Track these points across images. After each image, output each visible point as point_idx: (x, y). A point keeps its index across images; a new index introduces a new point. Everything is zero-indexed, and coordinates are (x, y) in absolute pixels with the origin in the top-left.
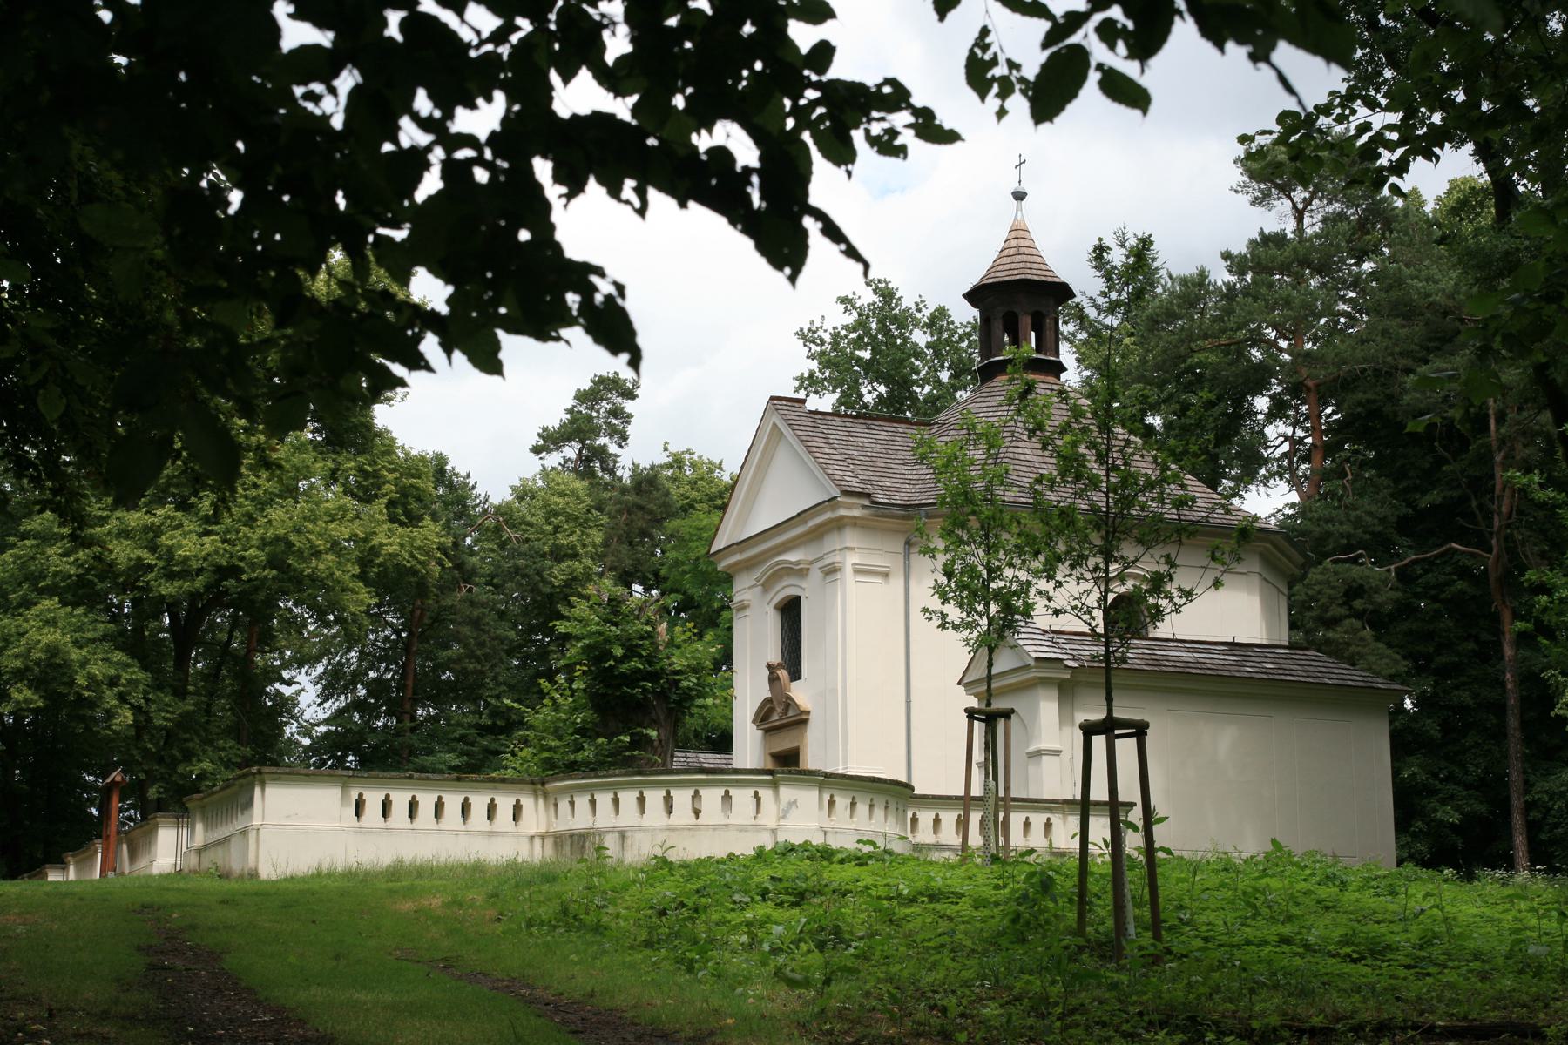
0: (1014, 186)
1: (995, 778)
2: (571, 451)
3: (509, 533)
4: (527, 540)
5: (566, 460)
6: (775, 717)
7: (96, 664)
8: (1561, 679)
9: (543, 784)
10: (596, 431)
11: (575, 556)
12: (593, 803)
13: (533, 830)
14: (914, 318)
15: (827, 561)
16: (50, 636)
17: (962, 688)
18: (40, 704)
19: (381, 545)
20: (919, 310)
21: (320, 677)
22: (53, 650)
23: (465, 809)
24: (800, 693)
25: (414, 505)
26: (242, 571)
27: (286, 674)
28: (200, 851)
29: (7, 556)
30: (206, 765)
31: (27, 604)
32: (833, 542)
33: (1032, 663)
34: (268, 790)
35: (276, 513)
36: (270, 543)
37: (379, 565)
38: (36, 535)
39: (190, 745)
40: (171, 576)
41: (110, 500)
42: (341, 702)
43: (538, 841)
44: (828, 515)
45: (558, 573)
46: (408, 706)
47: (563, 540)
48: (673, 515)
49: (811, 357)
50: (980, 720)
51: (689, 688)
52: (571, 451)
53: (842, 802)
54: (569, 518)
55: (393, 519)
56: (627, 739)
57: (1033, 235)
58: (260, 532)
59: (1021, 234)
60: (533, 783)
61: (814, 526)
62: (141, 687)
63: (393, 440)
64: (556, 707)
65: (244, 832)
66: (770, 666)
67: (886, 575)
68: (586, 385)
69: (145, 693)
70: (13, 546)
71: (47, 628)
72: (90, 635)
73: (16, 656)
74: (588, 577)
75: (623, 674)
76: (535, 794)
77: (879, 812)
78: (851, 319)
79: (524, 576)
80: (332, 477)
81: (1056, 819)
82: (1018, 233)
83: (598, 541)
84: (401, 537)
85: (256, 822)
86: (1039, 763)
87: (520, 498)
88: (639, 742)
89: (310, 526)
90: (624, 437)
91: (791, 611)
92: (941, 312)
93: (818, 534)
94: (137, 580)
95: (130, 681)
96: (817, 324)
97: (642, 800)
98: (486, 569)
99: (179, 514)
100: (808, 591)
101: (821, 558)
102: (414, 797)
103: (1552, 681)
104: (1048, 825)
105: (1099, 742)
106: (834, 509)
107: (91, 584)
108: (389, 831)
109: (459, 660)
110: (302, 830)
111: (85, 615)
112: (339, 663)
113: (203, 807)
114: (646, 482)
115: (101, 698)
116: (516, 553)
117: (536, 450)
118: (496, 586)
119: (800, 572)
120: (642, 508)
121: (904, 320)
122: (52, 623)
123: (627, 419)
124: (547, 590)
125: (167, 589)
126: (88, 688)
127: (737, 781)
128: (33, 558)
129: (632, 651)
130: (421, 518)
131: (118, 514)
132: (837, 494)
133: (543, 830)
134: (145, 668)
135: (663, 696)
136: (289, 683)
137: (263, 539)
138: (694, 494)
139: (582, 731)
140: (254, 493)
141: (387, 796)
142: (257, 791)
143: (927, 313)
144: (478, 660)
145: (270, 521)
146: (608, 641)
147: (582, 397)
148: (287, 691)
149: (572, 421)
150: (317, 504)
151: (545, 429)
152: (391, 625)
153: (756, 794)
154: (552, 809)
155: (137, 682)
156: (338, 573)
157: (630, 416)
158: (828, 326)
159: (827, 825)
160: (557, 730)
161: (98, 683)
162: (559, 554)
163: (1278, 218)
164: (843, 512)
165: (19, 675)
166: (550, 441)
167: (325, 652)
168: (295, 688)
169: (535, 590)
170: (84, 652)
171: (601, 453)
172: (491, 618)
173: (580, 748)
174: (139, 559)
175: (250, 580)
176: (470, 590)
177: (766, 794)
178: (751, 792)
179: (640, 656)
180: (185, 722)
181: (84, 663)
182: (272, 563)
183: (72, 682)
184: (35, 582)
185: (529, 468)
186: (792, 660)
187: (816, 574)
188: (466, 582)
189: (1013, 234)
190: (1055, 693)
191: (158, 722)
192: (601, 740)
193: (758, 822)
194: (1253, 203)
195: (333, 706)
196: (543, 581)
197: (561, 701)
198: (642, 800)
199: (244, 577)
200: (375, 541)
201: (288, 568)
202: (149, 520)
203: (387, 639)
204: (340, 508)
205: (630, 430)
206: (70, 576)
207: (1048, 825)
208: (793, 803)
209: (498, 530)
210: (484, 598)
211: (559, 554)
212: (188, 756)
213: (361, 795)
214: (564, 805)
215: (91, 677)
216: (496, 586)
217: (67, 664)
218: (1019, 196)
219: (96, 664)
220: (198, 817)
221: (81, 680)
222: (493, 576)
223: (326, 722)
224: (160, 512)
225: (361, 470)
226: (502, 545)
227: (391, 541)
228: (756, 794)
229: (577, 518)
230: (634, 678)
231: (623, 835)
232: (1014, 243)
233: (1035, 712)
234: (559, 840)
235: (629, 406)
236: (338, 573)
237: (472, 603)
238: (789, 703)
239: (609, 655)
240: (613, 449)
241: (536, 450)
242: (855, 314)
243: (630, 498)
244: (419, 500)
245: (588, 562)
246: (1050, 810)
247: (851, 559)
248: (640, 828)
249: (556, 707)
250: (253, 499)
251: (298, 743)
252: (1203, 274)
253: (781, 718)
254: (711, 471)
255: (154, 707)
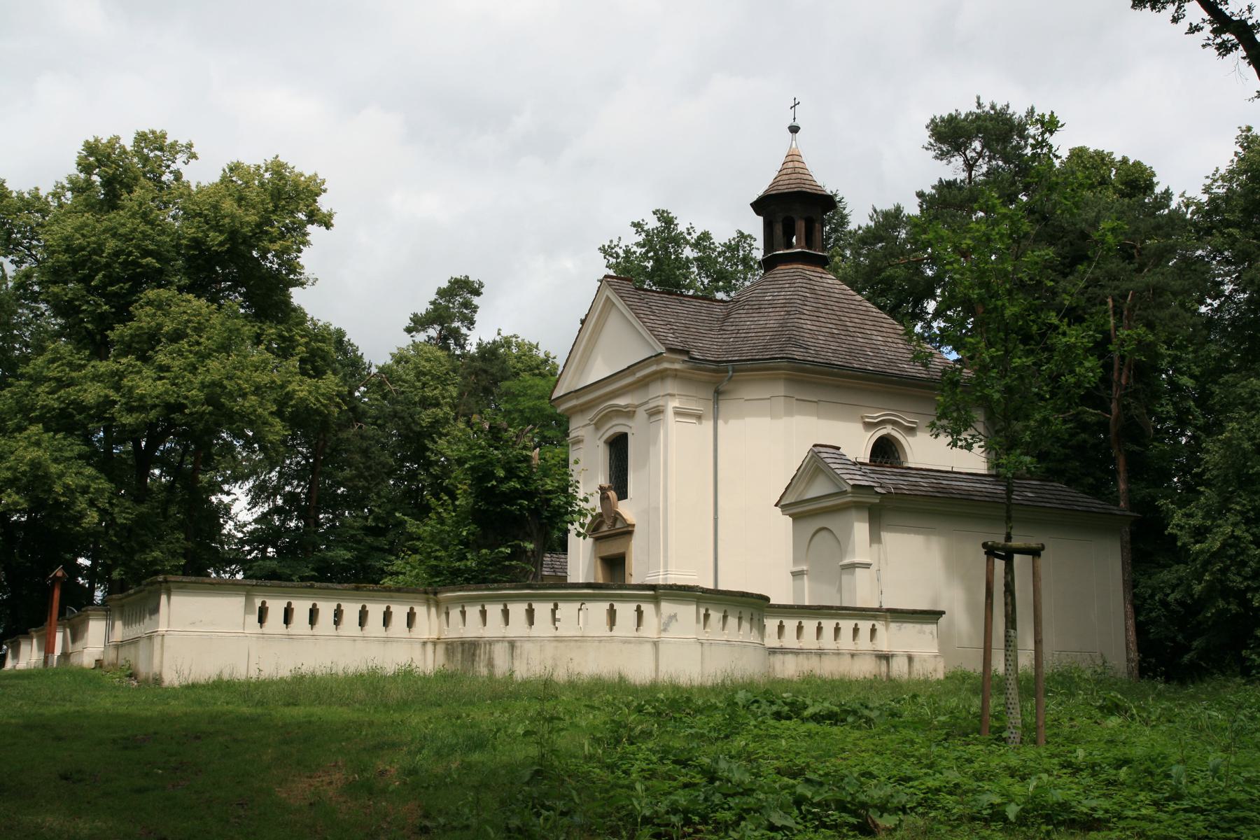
0: (790, 122)
1: (1011, 621)
2: (433, 332)
3: (390, 387)
4: (403, 392)
5: (430, 338)
6: (605, 528)
7: (74, 476)
8: (1171, 506)
9: (435, 594)
10: (451, 318)
11: (437, 405)
12: (483, 613)
13: (426, 636)
14: (684, 238)
15: (652, 405)
16: (33, 454)
17: (778, 509)
18: (25, 506)
19: (294, 391)
20: (689, 234)
21: (250, 490)
22: (35, 465)
23: (363, 617)
24: (627, 510)
25: (319, 363)
26: (185, 406)
27: (226, 487)
28: (118, 646)
29: (6, 392)
30: (157, 554)
31: (20, 429)
32: (656, 390)
33: (849, 489)
34: (173, 598)
35: (213, 364)
36: (208, 387)
37: (292, 406)
38: (30, 378)
39: (145, 538)
40: (130, 410)
41: (87, 352)
42: (265, 508)
43: (430, 647)
44: (654, 368)
45: (426, 417)
46: (312, 513)
47: (428, 393)
48: (506, 379)
49: (609, 266)
50: (1000, 557)
51: (559, 506)
52: (433, 332)
53: (715, 616)
54: (434, 377)
55: (304, 372)
56: (509, 551)
57: (804, 159)
58: (200, 378)
59: (796, 158)
60: (426, 592)
61: (638, 378)
62: (107, 494)
63: (306, 315)
64: (442, 521)
65: (150, 638)
66: (601, 488)
67: (699, 417)
68: (445, 285)
69: (110, 499)
70: (10, 385)
71: (30, 448)
72: (67, 454)
73: (8, 469)
74: (447, 421)
75: (503, 493)
76: (428, 603)
77: (732, 621)
78: (640, 238)
79: (402, 418)
80: (257, 340)
81: (880, 626)
82: (793, 157)
83: (455, 395)
84: (310, 386)
85: (162, 628)
86: (853, 574)
87: (398, 362)
88: (518, 553)
89: (239, 373)
90: (472, 323)
91: (618, 447)
92: (705, 236)
93: (644, 383)
94: (105, 412)
95: (97, 490)
96: (615, 243)
97: (530, 613)
98: (373, 412)
99: (139, 363)
100: (635, 430)
101: (646, 403)
102: (314, 605)
103: (1164, 508)
104: (873, 631)
105: (999, 565)
106: (658, 363)
107: (72, 416)
108: (290, 637)
109: (351, 480)
110: (206, 639)
111: (65, 439)
112: (264, 480)
113: (122, 606)
114: (489, 353)
115: (74, 503)
116: (394, 402)
117: (409, 330)
118: (379, 426)
119: (629, 413)
120: (485, 372)
121: (678, 240)
122: (38, 444)
123: (475, 309)
124: (418, 429)
125: (128, 420)
126: (63, 495)
127: (621, 596)
128: (27, 395)
129: (511, 473)
130: (325, 373)
131: (93, 363)
132: (663, 349)
133: (435, 636)
134: (111, 480)
135: (536, 512)
136: (228, 493)
137: (202, 383)
138: (519, 365)
139: (466, 543)
140: (196, 348)
141: (289, 604)
142: (164, 598)
143: (695, 236)
144: (366, 479)
145: (208, 370)
146: (490, 463)
147: (441, 293)
148: (226, 499)
149: (435, 310)
150: (245, 357)
151: (415, 315)
152: (301, 453)
153: (639, 608)
154: (444, 616)
155: (103, 490)
156: (260, 410)
157: (476, 307)
158: (622, 244)
159: (703, 637)
160: (442, 540)
161: (73, 492)
162: (426, 403)
163: (953, 169)
164: (666, 365)
165: (11, 483)
166: (418, 324)
167: (253, 472)
168: (232, 497)
169: (408, 427)
170: (61, 467)
171: (456, 334)
172: (375, 449)
173: (463, 557)
174: (107, 396)
175: (191, 414)
176: (361, 427)
177: (648, 608)
178: (634, 606)
179: (519, 477)
180: (141, 521)
181: (61, 475)
182: (209, 401)
183: (50, 491)
184: (25, 412)
185: (404, 341)
186: (619, 482)
187: (641, 414)
188: (358, 421)
189: (790, 158)
190: (866, 515)
191: (120, 521)
192: (484, 551)
193: (640, 634)
194: (936, 157)
195: (258, 511)
196: (414, 422)
197: (444, 515)
198: (530, 613)
199: (187, 411)
200: (290, 388)
201: (220, 409)
202: (115, 367)
203: (298, 463)
204: (263, 361)
205: (476, 317)
206: (54, 409)
207: (873, 631)
208: (673, 617)
209: (381, 384)
210: (371, 433)
211: (426, 403)
212: (144, 547)
213: (264, 603)
214: (455, 613)
215: (67, 487)
216: (379, 426)
217: (47, 475)
218: (794, 130)
219: (74, 476)
220: (117, 615)
221: (58, 488)
222: (377, 418)
223: (256, 521)
224: (124, 360)
225: (281, 336)
226: (384, 397)
227: (302, 389)
228: (639, 608)
229: (439, 377)
230: (514, 495)
231: (512, 645)
232: (790, 165)
233: (849, 532)
234: (451, 647)
235: (476, 300)
236: (260, 410)
237: (363, 437)
238: (617, 517)
239: (491, 476)
240: (464, 330)
241: (409, 330)
242: (643, 235)
243: (478, 364)
244: (323, 359)
245: (447, 409)
246: (874, 617)
247: (673, 404)
248: (529, 639)
249: (442, 521)
250: (196, 354)
251: (234, 536)
252: (898, 209)
253: (612, 533)
254: (531, 350)
255: (117, 510)
